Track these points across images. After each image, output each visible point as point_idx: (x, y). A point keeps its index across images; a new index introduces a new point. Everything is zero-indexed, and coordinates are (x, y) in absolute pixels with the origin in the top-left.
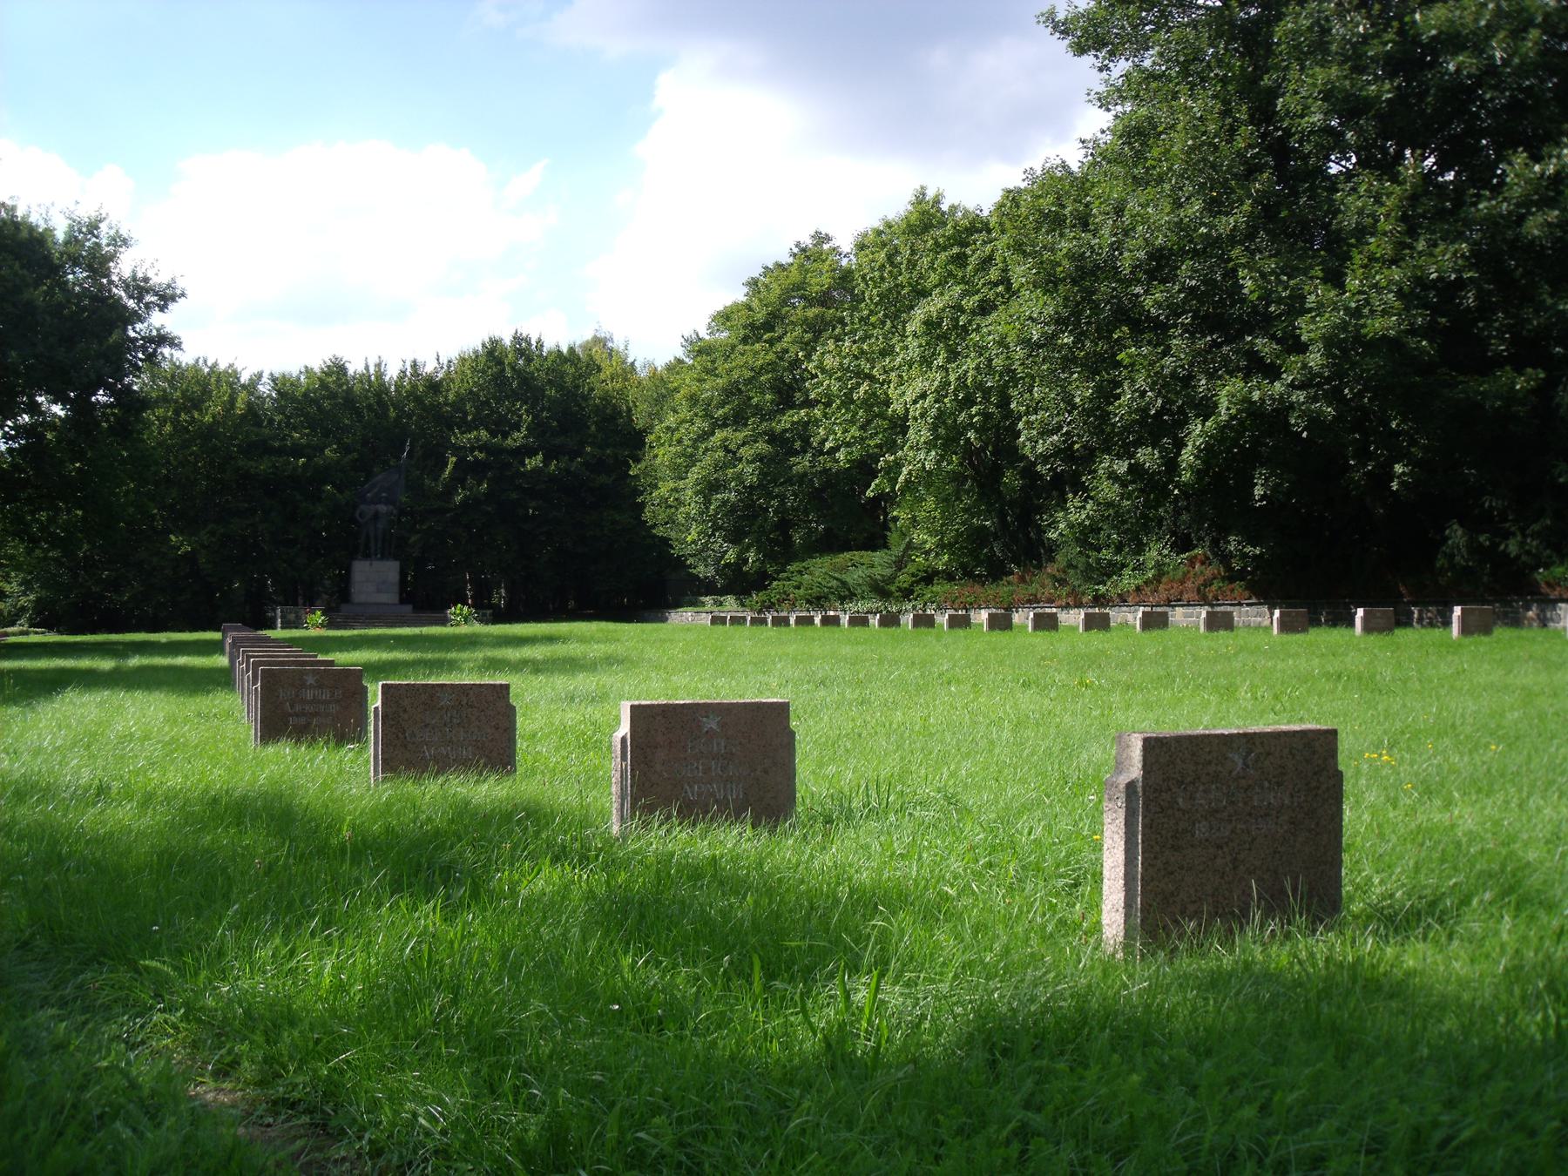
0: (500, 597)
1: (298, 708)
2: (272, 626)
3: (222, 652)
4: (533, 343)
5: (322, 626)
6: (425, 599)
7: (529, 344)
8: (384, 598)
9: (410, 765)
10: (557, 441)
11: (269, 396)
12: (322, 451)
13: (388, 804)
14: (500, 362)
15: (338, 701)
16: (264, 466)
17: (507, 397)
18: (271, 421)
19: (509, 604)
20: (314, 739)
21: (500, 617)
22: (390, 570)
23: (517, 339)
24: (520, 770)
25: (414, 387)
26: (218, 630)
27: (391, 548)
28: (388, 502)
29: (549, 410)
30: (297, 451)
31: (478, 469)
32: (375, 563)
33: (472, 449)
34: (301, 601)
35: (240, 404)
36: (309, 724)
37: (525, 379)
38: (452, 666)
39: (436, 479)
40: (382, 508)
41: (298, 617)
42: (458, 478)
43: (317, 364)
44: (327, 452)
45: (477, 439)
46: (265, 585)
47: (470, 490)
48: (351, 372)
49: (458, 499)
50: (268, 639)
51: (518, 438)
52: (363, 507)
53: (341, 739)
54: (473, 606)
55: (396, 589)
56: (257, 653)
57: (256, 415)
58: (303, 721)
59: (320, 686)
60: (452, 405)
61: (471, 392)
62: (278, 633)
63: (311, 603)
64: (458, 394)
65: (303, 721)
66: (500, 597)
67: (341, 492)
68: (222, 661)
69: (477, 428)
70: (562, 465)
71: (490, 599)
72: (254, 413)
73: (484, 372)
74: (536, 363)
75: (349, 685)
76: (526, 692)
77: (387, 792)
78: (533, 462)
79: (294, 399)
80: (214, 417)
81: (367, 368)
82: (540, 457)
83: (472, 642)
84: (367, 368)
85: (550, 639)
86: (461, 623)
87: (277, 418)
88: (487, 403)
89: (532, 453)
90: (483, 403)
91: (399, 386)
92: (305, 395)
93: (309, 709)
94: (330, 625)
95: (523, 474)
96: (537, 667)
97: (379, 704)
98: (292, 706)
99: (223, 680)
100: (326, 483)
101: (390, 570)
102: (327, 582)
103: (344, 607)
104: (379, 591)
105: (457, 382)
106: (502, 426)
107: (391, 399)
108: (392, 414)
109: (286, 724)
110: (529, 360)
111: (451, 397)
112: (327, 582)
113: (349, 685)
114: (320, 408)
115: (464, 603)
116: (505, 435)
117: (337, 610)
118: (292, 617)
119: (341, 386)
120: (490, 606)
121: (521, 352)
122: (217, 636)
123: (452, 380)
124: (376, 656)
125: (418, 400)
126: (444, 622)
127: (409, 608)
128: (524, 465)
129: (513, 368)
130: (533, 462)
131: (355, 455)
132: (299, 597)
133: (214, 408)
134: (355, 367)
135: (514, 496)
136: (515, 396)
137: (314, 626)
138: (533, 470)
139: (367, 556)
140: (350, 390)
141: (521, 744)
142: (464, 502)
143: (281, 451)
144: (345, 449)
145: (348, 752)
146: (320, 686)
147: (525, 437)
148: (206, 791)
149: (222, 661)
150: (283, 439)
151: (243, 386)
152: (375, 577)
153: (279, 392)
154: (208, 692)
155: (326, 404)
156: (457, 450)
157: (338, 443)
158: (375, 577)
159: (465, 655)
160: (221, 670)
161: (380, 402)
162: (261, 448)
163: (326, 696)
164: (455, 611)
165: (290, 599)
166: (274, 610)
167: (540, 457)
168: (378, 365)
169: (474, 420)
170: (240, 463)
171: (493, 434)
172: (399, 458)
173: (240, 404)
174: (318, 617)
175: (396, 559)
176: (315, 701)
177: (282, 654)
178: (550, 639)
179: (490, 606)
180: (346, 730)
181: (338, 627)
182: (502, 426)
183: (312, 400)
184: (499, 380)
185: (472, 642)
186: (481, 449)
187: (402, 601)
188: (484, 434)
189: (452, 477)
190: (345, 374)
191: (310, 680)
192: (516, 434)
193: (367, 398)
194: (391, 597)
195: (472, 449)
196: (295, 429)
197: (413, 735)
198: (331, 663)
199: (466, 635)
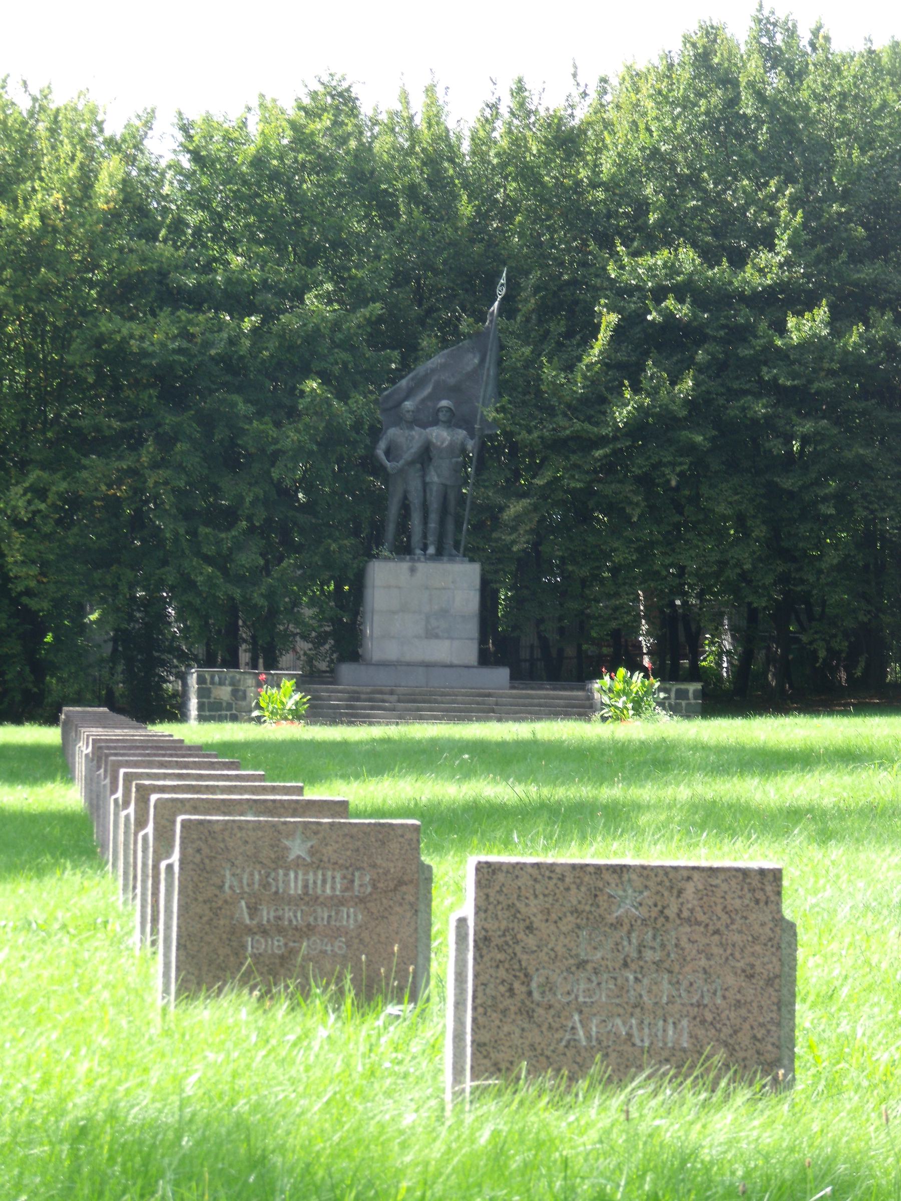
0: (719, 651)
1: (266, 914)
2: (177, 714)
3: (66, 772)
4: (804, 37)
5: (297, 716)
6: (542, 651)
7: (791, 33)
8: (441, 651)
9: (542, 1061)
10: (866, 273)
11: (176, 167)
12: (298, 296)
13: (498, 1154)
14: (728, 81)
15: (362, 900)
16: (156, 335)
17: (745, 166)
18: (178, 225)
19: (742, 671)
20: (305, 992)
21: (719, 700)
22: (456, 584)
23: (765, 25)
24: (803, 1078)
25: (518, 142)
26: (52, 720)
27: (463, 530)
28: (454, 420)
29: (845, 197)
30: (239, 299)
31: (672, 341)
32: (424, 568)
33: (659, 294)
34: (244, 657)
35: (105, 188)
36: (293, 952)
37: (786, 120)
38: (616, 817)
39: (569, 368)
40: (441, 436)
41: (239, 694)
42: (623, 368)
43: (290, 94)
44: (311, 299)
45: (672, 269)
46: (162, 617)
47: (653, 393)
48: (366, 109)
49: (621, 415)
50: (177, 747)
51: (766, 267)
52: (393, 432)
53: (369, 992)
54: (658, 673)
55: (472, 628)
56: (165, 783)
57: (142, 211)
58: (276, 945)
59: (316, 862)
60: (610, 186)
61: (655, 153)
62: (192, 731)
63: (268, 658)
64: (623, 159)
65: (276, 945)
66: (719, 651)
67: (343, 396)
68: (65, 796)
69: (668, 242)
70: (878, 333)
71: (695, 652)
72: (135, 209)
73: (686, 104)
74: (813, 81)
75: (382, 870)
76: (820, 891)
77: (491, 1120)
78: (807, 326)
79: (230, 174)
80: (43, 217)
81: (405, 99)
82: (822, 313)
83: (658, 761)
84: (405, 99)
85: (849, 757)
86: (627, 714)
87: (195, 218)
88: (693, 181)
89: (803, 302)
90: (684, 181)
91: (480, 145)
92: (258, 162)
93: (292, 916)
94: (316, 712)
95: (782, 355)
96: (824, 825)
97: (468, 910)
98: (253, 910)
99: (72, 841)
100: (307, 372)
101: (456, 584)
102: (308, 612)
103: (347, 670)
104: (431, 634)
105: (623, 128)
106: (731, 238)
107: (462, 173)
108: (466, 208)
109: (239, 952)
110: (796, 76)
111: (607, 167)
112: (308, 612)
113: (382, 870)
114: (293, 196)
115: (634, 666)
116: (739, 260)
117: (331, 677)
118: (224, 693)
119: (343, 141)
120: (696, 673)
121: (773, 58)
122: (47, 735)
123: (608, 125)
124: (476, 790)
125: (528, 175)
126: (584, 709)
127: (504, 673)
128: (782, 330)
129: (760, 95)
130: (807, 326)
131: (377, 307)
132: (243, 640)
133: (47, 197)
134: (375, 100)
135: (760, 409)
136: (766, 165)
137: (278, 716)
138: (804, 346)
139: (403, 550)
140: (364, 152)
141: (805, 1016)
142: (638, 428)
143: (197, 299)
144: (354, 295)
145: (389, 1019)
146: (316, 862)
147: (788, 263)
148: (59, 1111)
149: (65, 796)
150: (207, 268)
151: (110, 142)
152: (423, 601)
153: (196, 157)
154: (40, 872)
155: (308, 185)
156: (621, 293)
157: (338, 277)
158: (423, 601)
159: (645, 792)
160: (66, 819)
161: (437, 180)
162: (150, 290)
163: (331, 885)
164: (610, 686)
165: (221, 653)
166: (182, 677)
167: (822, 313)
168: (520, 89)
169: (662, 224)
170: (105, 326)
171: (709, 256)
172: (481, 317)
173: (105, 188)
174: (286, 694)
175: (471, 554)
176: (308, 898)
177: (220, 783)
178: (849, 757)
179: (696, 673)
180: (384, 973)
181: (334, 718)
182: (731, 238)
183: (275, 176)
184: (727, 125)
185: (658, 761)
186: (680, 293)
187: (485, 659)
188: (688, 257)
189: (608, 363)
190: (353, 112)
191: (297, 849)
192: (764, 257)
193: (405, 169)
194: (462, 647)
195: (659, 294)
196: (233, 243)
197: (548, 986)
198: (341, 807)
199: (644, 746)
